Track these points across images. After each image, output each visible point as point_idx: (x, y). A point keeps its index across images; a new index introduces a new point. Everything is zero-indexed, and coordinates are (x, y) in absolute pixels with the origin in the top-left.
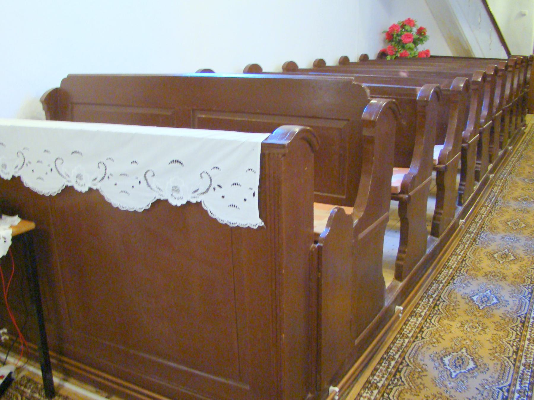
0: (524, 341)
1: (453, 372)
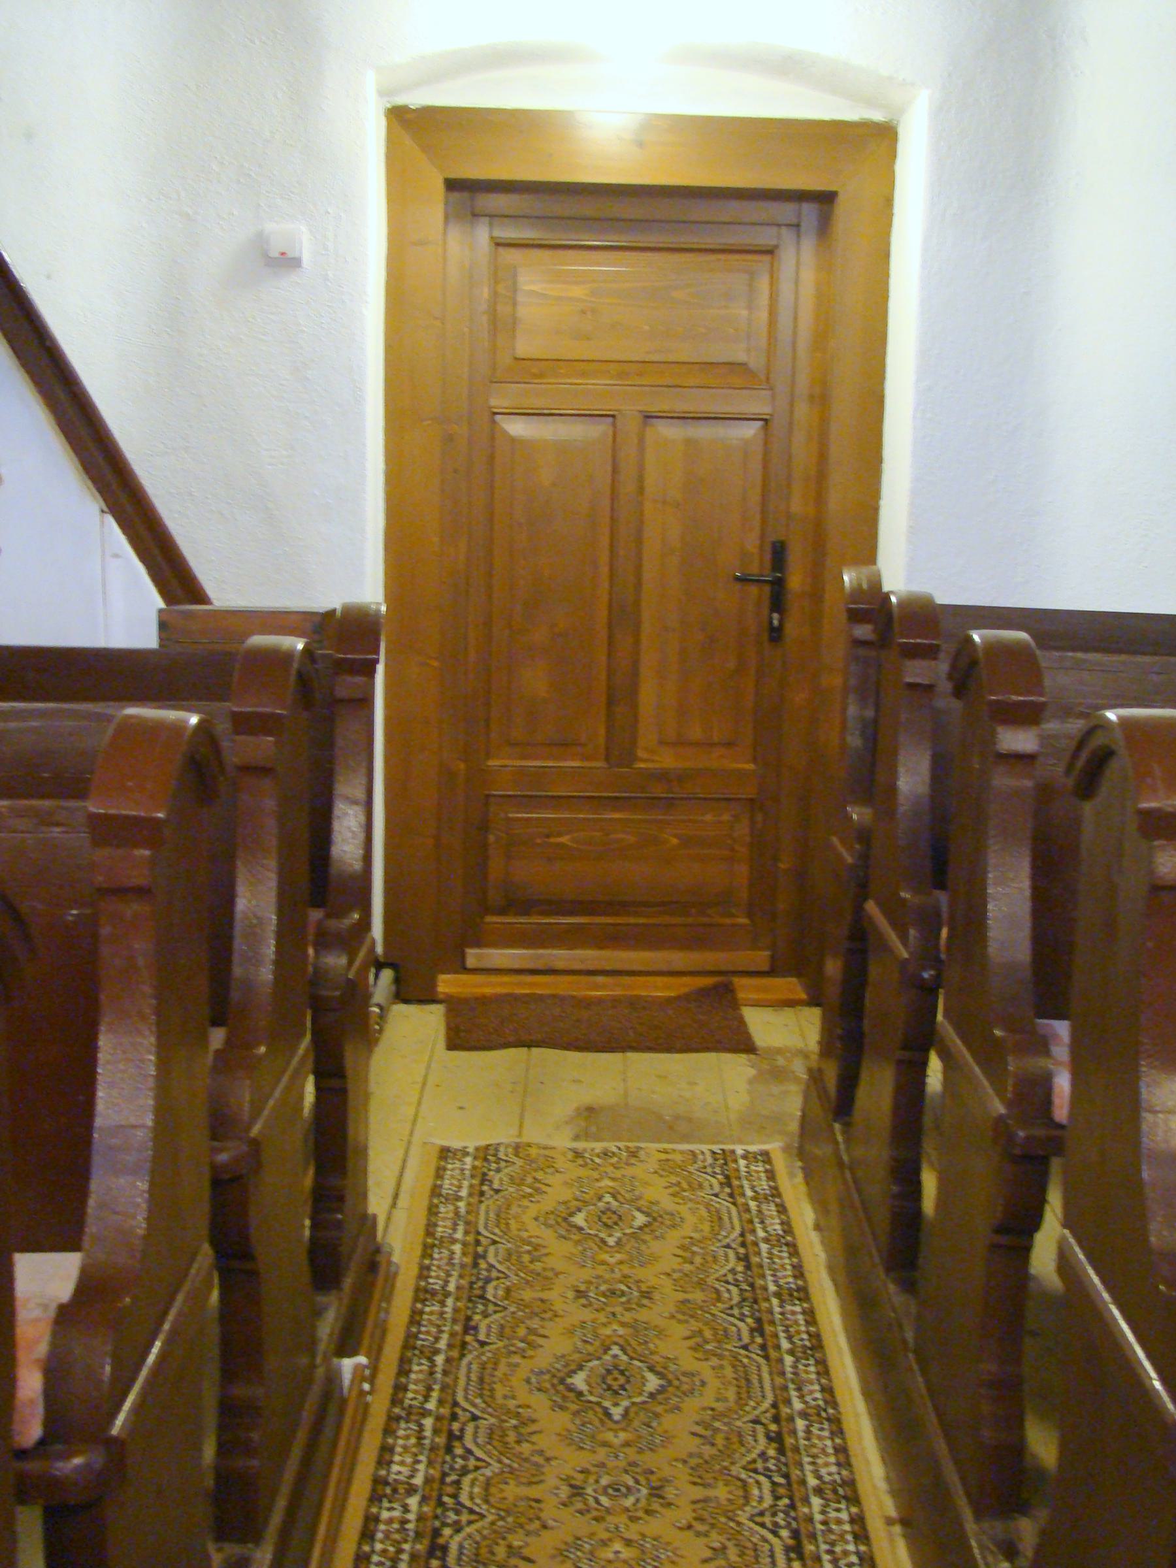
0: (806, 1501)
1: (612, 1408)
